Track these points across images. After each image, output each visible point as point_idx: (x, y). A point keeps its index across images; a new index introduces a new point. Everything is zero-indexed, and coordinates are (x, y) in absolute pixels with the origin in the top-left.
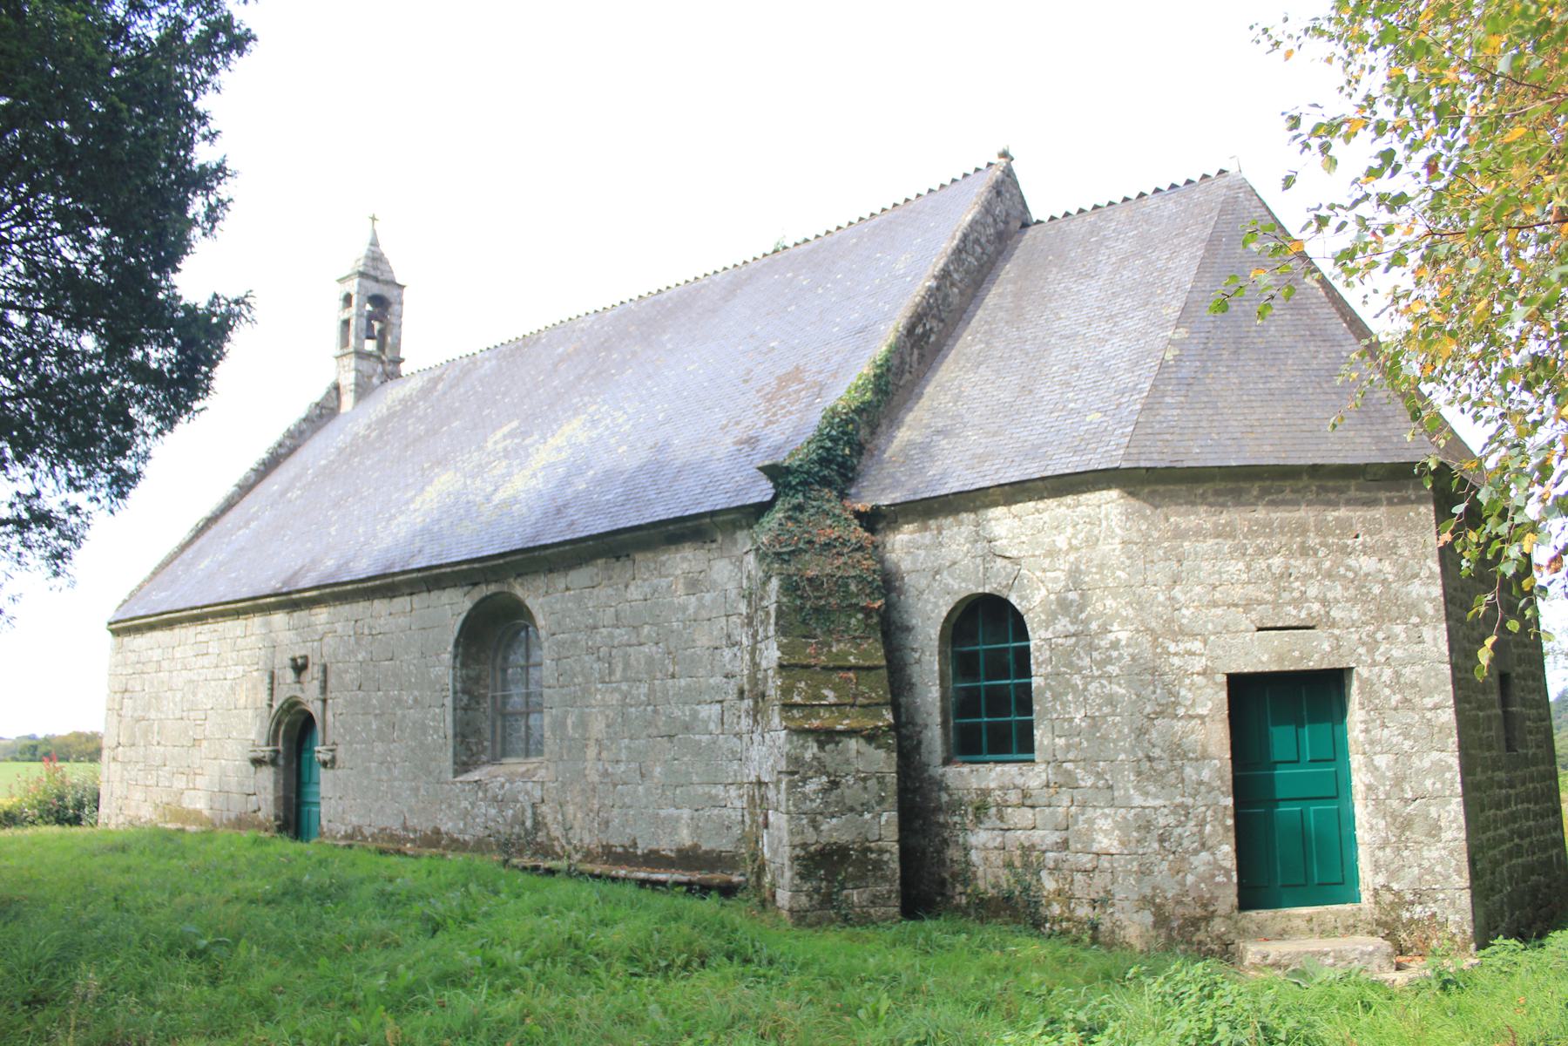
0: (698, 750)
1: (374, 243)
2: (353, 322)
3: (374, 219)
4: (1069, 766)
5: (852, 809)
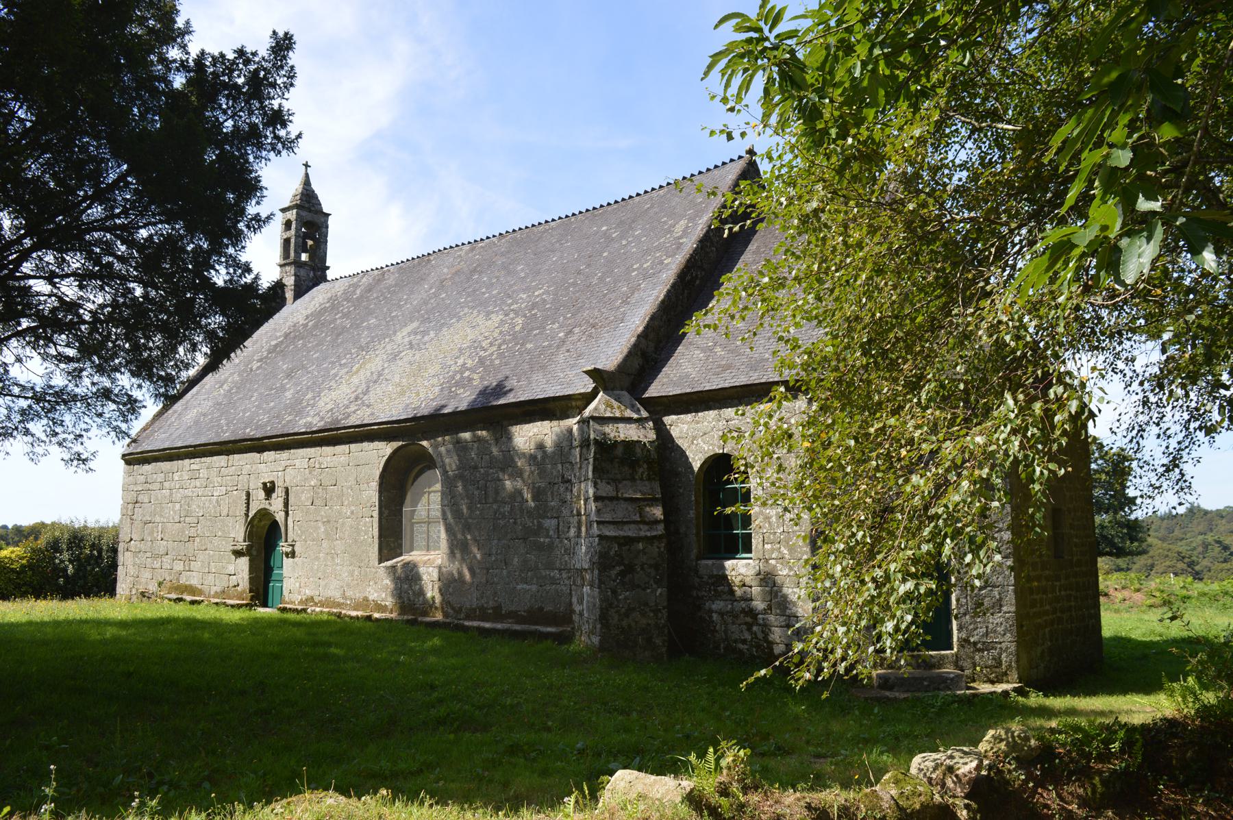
0: (540, 547)
1: (307, 182)
2: (293, 241)
3: (307, 166)
4: (772, 562)
5: (639, 586)
